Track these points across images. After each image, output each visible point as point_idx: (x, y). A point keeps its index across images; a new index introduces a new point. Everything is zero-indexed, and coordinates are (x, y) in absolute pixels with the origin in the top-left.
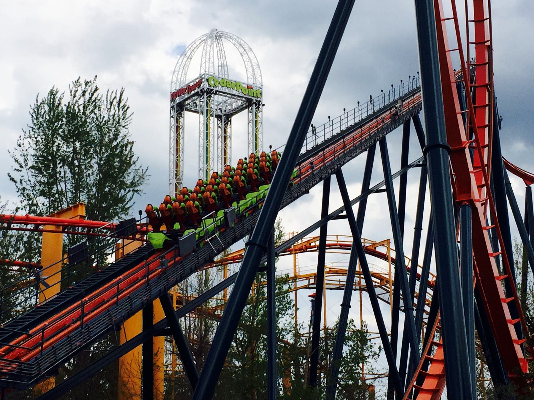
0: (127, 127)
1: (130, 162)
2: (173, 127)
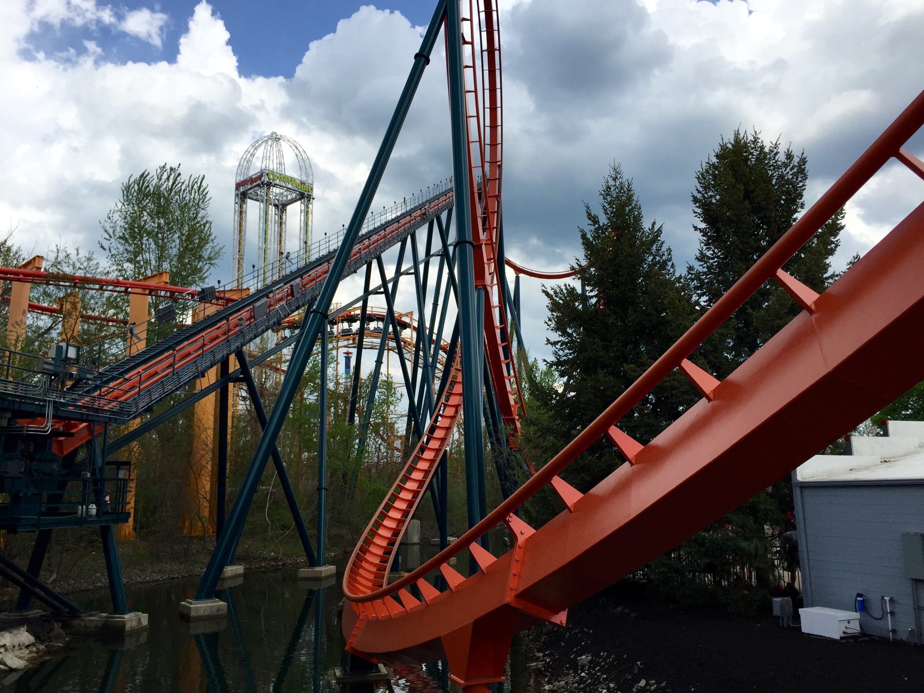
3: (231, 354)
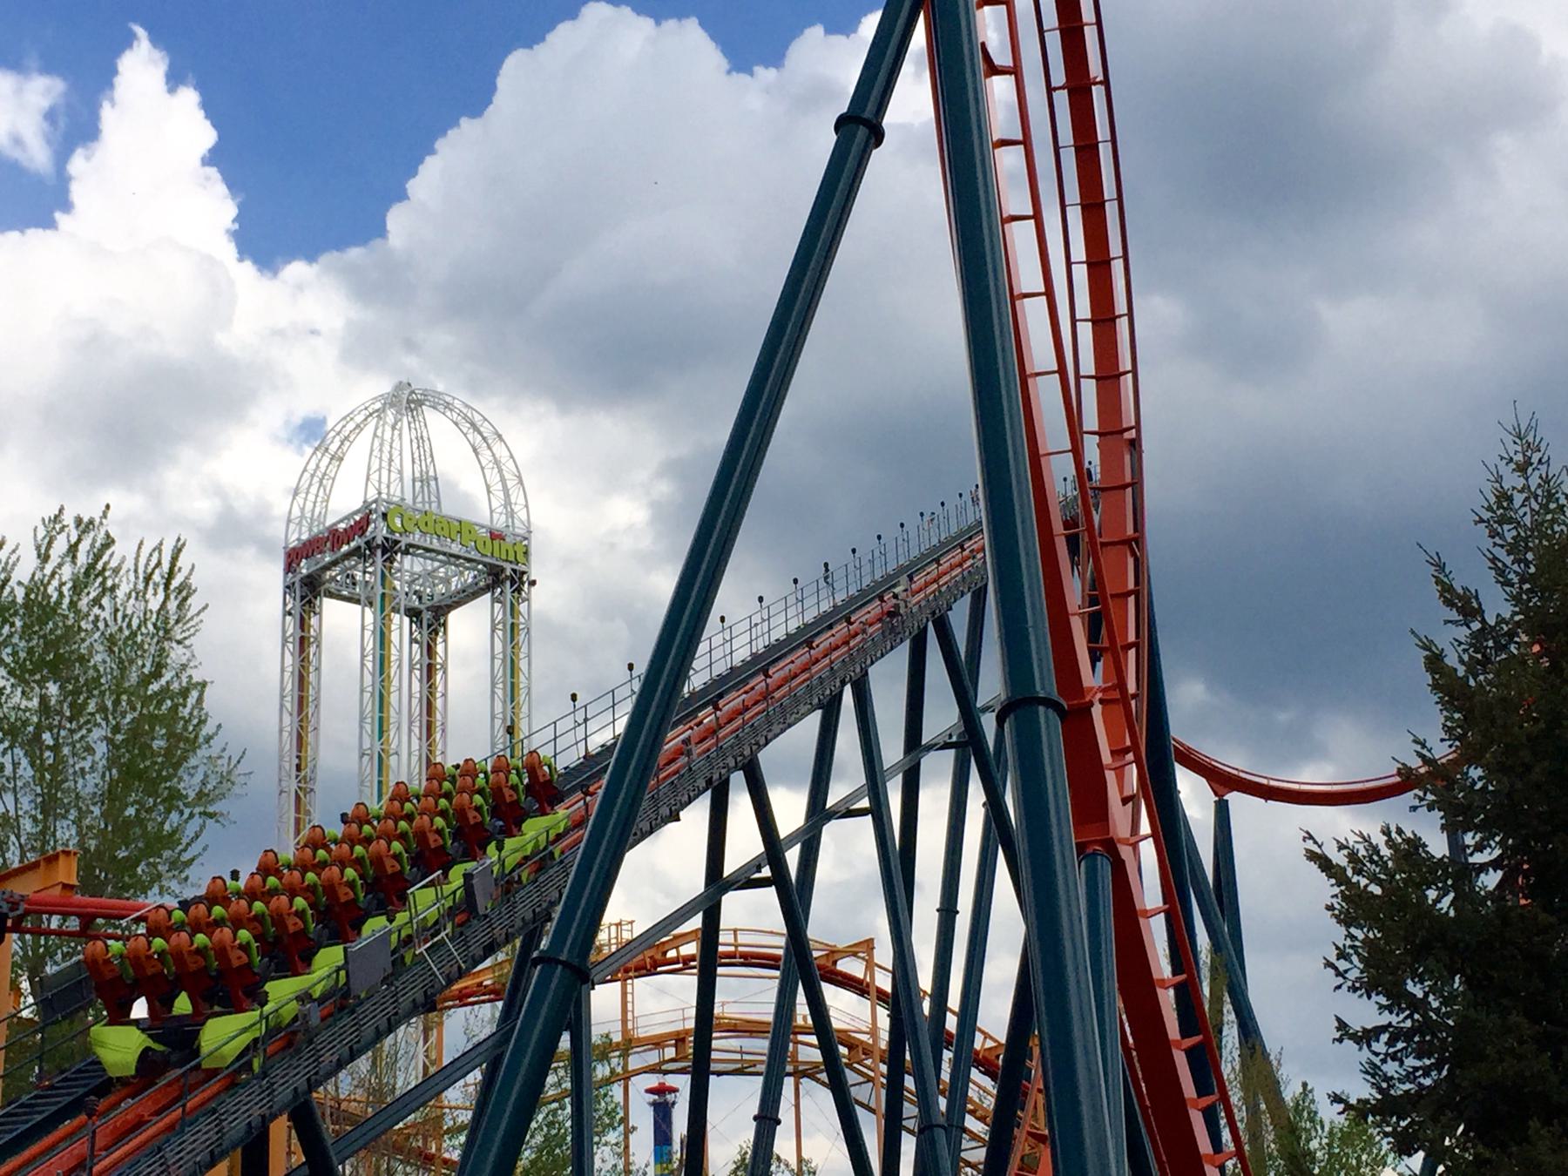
0: (187, 642)
1: (196, 737)
2: (291, 639)
3: (274, 1117)
